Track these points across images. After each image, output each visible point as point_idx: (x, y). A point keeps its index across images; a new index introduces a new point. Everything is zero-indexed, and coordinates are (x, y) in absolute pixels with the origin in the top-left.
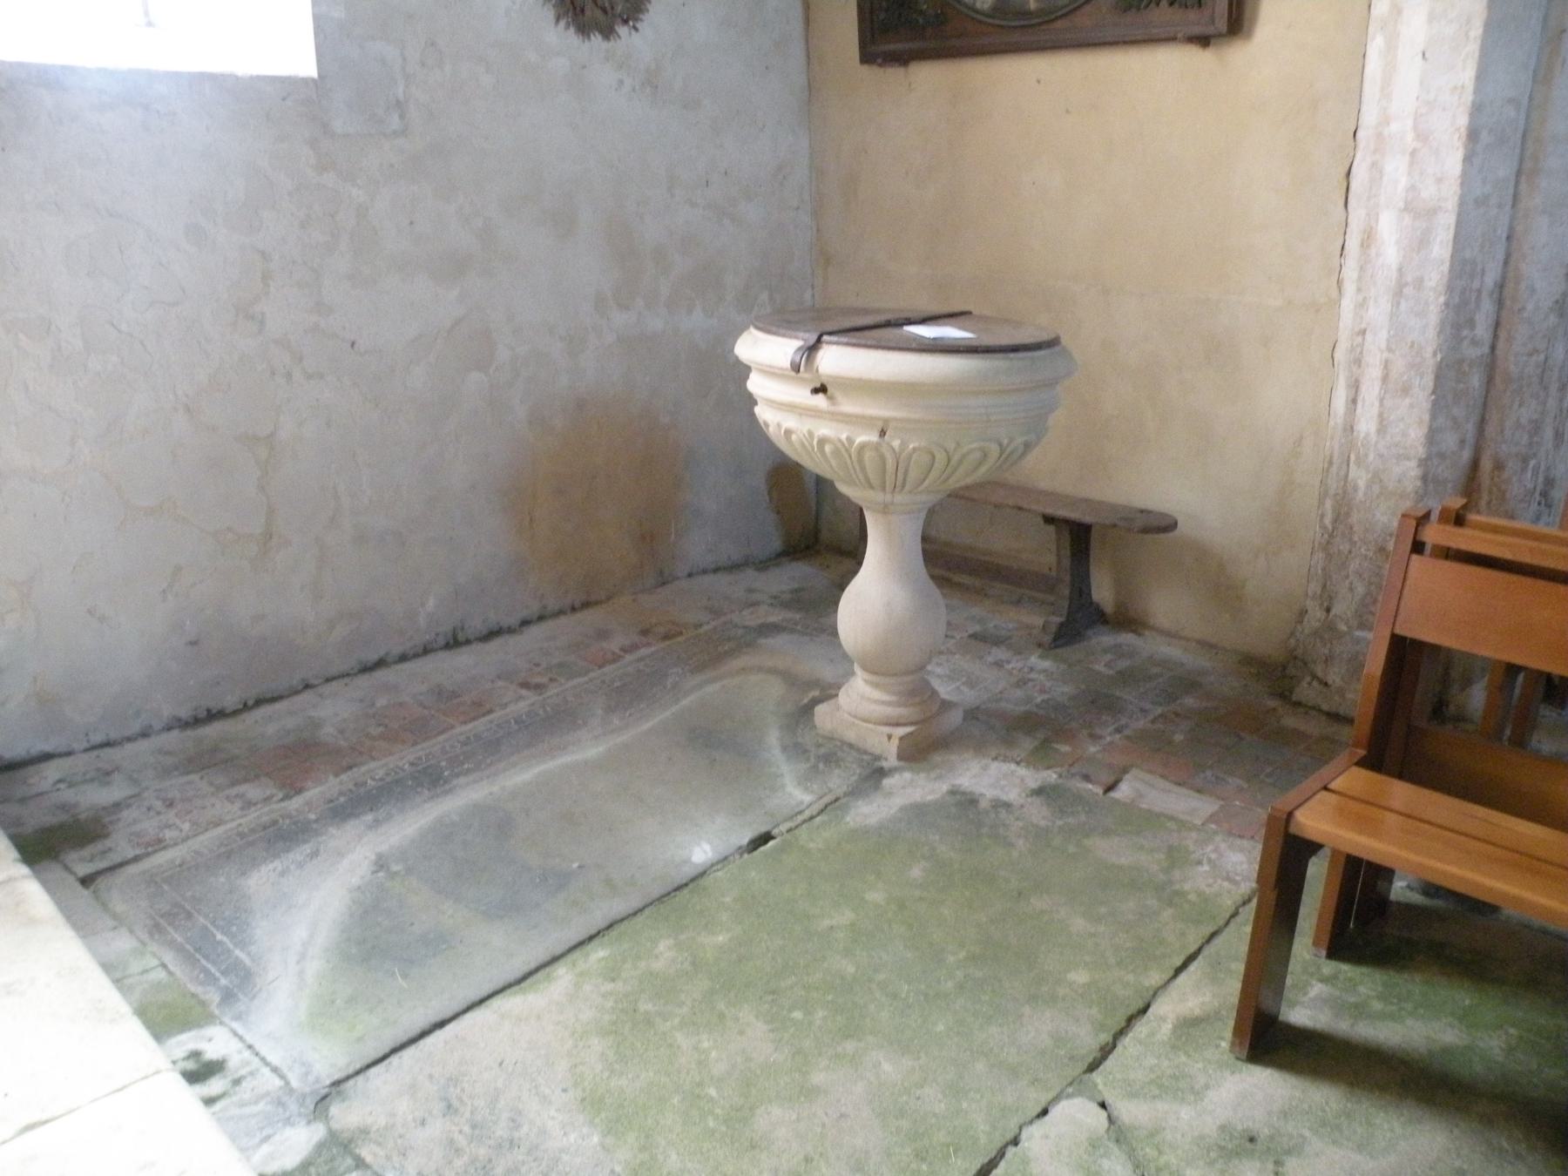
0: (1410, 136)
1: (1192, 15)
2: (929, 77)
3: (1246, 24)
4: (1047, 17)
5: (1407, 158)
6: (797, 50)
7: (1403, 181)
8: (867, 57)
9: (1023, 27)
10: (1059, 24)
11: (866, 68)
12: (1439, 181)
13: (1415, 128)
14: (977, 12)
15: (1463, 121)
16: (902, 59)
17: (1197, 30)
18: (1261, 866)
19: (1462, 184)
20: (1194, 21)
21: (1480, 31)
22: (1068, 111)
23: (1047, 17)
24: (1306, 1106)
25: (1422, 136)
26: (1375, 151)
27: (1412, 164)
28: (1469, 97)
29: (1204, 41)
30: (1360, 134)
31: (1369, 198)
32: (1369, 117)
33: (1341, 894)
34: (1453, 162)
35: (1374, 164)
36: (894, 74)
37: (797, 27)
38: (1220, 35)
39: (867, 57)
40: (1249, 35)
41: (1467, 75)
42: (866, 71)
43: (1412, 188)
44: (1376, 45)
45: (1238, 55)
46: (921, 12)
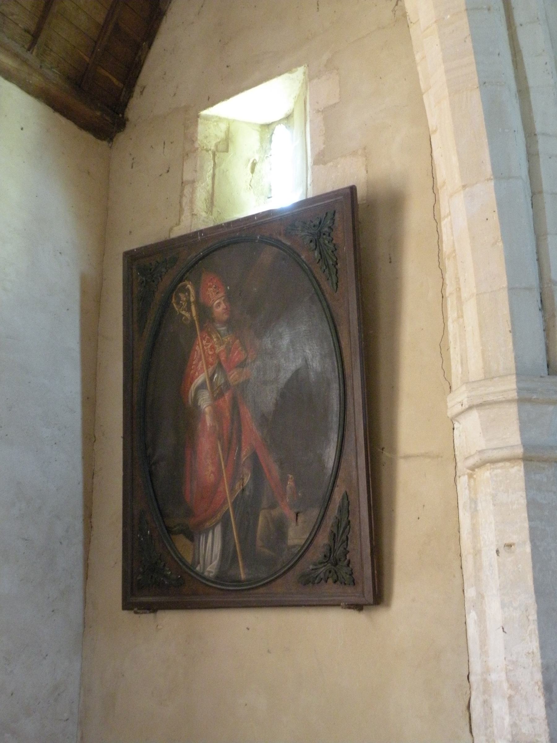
0: (505, 685)
1: (349, 590)
2: (171, 621)
3: (385, 598)
4: (252, 585)
5: (506, 701)
6: (77, 598)
7: (507, 720)
8: (127, 605)
9: (236, 590)
10: (261, 590)
11: (126, 612)
12: (532, 720)
13: (508, 680)
14: (204, 578)
15: (539, 677)
16: (152, 608)
17: (354, 600)
18: (124, 420)
19: (549, 724)
20: (354, 597)
21: (535, 617)
22: (269, 651)
23: (252, 585)
24: (506, 131)
25: (514, 686)
26: (484, 692)
27: (510, 706)
28: (538, 660)
29: (359, 607)
30: (472, 678)
31: (486, 728)
32: (476, 667)
33: (511, 47)
34: (538, 706)
35: (485, 702)
36: (147, 618)
37: (78, 582)
38: (369, 604)
39: (127, 605)
40: (388, 605)
41: (534, 645)
42: (128, 615)
43: (514, 725)
44: (472, 617)
45: (382, 617)
46: (166, 576)
